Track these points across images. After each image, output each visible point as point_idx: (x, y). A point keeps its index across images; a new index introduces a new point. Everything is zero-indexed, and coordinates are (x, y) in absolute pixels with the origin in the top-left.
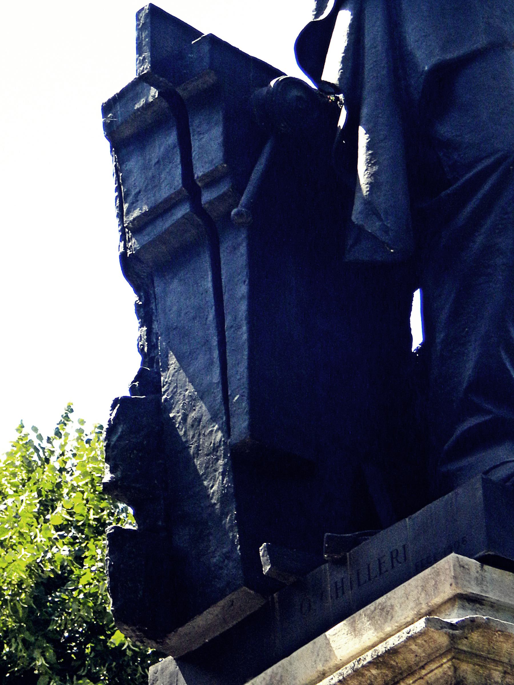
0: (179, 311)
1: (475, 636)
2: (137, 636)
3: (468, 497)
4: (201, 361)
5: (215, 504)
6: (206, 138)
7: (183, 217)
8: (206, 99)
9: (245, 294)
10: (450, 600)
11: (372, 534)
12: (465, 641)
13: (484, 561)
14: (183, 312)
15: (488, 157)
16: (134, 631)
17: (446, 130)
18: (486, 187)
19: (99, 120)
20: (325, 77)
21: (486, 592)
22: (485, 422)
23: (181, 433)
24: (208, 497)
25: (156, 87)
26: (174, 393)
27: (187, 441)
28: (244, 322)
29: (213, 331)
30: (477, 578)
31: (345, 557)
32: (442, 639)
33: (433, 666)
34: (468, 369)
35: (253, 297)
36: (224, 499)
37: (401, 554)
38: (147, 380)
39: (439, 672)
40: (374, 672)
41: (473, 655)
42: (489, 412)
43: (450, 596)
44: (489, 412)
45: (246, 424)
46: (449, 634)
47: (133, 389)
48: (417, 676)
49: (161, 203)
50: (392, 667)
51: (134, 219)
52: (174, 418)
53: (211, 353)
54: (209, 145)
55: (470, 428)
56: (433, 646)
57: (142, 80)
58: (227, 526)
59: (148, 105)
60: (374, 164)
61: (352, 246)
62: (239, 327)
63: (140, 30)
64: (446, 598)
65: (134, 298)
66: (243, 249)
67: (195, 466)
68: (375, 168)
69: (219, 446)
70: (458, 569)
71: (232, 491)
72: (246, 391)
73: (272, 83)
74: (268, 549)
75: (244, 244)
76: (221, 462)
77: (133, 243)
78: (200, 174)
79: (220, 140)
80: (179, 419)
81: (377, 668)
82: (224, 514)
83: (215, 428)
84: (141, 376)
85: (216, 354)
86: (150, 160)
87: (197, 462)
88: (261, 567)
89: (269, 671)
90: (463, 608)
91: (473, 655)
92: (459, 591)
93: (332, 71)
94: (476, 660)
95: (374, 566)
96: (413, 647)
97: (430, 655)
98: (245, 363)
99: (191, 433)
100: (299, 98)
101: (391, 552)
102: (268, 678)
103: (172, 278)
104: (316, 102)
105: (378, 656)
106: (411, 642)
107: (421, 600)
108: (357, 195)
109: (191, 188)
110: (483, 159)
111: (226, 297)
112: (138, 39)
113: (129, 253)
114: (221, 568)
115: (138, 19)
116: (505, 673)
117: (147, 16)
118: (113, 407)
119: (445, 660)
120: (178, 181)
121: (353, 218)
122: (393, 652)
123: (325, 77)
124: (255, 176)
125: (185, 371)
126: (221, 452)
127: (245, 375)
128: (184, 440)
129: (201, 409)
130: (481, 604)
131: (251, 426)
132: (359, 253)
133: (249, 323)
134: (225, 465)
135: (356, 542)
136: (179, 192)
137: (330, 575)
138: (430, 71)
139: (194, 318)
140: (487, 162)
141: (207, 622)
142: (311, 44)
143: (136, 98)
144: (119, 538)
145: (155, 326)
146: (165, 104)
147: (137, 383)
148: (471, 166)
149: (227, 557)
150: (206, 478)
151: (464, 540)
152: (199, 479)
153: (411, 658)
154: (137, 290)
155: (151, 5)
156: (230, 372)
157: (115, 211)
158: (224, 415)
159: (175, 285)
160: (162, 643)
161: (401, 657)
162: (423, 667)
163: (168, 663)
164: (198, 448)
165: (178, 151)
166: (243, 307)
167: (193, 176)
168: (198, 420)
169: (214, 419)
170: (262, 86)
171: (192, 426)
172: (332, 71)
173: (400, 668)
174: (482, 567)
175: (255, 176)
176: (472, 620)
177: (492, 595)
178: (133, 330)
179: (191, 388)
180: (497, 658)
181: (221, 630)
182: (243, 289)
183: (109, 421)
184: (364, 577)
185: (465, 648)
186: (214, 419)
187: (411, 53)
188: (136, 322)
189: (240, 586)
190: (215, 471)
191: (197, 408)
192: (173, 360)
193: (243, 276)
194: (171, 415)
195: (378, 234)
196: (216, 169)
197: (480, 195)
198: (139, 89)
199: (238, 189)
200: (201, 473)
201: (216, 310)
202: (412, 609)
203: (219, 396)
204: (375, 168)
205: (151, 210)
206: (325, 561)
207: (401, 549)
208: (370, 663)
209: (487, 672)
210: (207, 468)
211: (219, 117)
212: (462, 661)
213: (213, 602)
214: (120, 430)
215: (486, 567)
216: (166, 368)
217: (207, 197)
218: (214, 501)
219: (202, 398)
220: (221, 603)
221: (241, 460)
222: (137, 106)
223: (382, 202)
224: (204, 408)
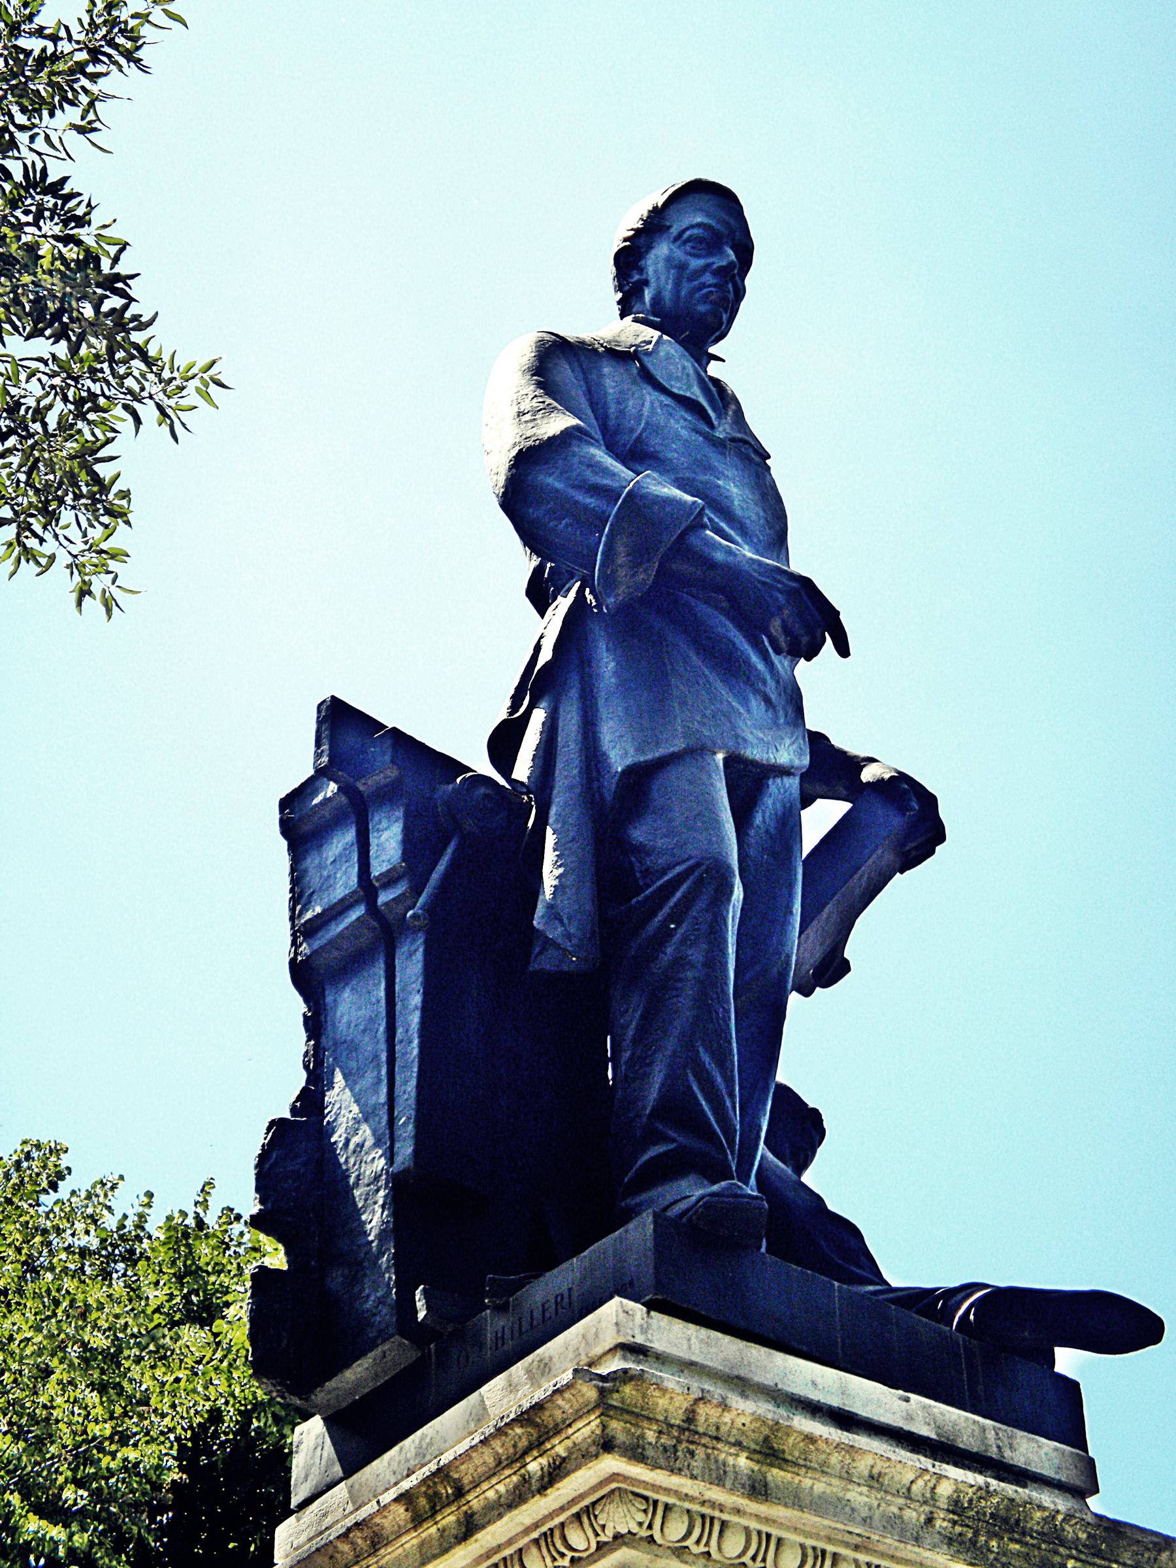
0: (349, 1023)
1: (628, 1390)
2: (278, 1391)
3: (639, 1233)
4: (369, 1078)
5: (372, 1241)
6: (385, 835)
7: (358, 919)
8: (387, 796)
9: (419, 1005)
10: (610, 1350)
11: (537, 1277)
12: (616, 1396)
13: (651, 1306)
14: (353, 1025)
15: (684, 861)
16: (274, 1385)
17: (639, 834)
18: (679, 894)
19: (276, 816)
20: (516, 775)
21: (651, 1341)
22: (666, 1153)
23: (342, 1160)
24: (366, 1234)
25: (335, 782)
26: (337, 1115)
27: (347, 1170)
28: (416, 1035)
29: (383, 1046)
30: (641, 1326)
31: (507, 1303)
32: (590, 1393)
33: (579, 1424)
34: (653, 1093)
35: (426, 1008)
36: (382, 1236)
37: (566, 1300)
38: (311, 1101)
39: (586, 1431)
40: (519, 1431)
41: (624, 1411)
42: (674, 1140)
43: (612, 1346)
44: (674, 1140)
45: (410, 1150)
46: (596, 1386)
47: (293, 1110)
48: (564, 1436)
49: (336, 904)
50: (537, 1426)
51: (306, 922)
52: (335, 1142)
53: (379, 1071)
54: (388, 842)
55: (652, 1158)
56: (581, 1400)
57: (321, 773)
58: (384, 1266)
59: (326, 800)
60: (560, 866)
61: (540, 953)
62: (410, 1042)
63: (320, 722)
64: (607, 1348)
65: (303, 1008)
66: (419, 955)
67: (354, 1198)
68: (561, 870)
69: (381, 1175)
70: (622, 1315)
71: (391, 1226)
72: (413, 1112)
73: (458, 780)
74: (424, 1291)
75: (421, 950)
76: (382, 1193)
77: (304, 948)
78: (377, 874)
79: (400, 838)
80: (340, 1145)
81: (522, 1427)
82: (381, 1253)
83: (378, 1156)
84: (304, 1095)
85: (384, 1071)
86: (326, 859)
87: (357, 1193)
88: (416, 1312)
89: (419, 1433)
90: (624, 1358)
91: (624, 1411)
92: (621, 1340)
93: (522, 770)
94: (627, 1417)
95: (537, 1314)
96: (560, 1402)
97: (577, 1411)
98: (413, 1083)
99: (352, 1161)
100: (486, 796)
101: (556, 1297)
102: (417, 1442)
103: (344, 987)
104: (507, 802)
105: (522, 1413)
106: (557, 1396)
107: (581, 1350)
108: (541, 897)
109: (367, 887)
110: (674, 867)
111: (398, 1007)
112: (317, 731)
113: (299, 958)
114: (374, 1315)
115: (319, 711)
116: (660, 1432)
117: (328, 707)
118: (269, 1129)
119: (593, 1417)
120: (354, 880)
121: (535, 922)
122: (538, 1407)
123: (516, 775)
124: (435, 876)
125: (351, 1090)
126: (382, 1182)
127: (413, 1094)
128: (344, 1167)
129: (366, 1131)
130: (646, 1355)
131: (416, 1152)
132: (545, 962)
133: (419, 1037)
134: (386, 1197)
135: (520, 1285)
136: (354, 892)
137: (492, 1324)
138: (623, 771)
139: (364, 1031)
140: (678, 869)
141: (357, 1375)
142: (504, 743)
143: (315, 793)
144: (263, 1276)
145: (323, 1040)
146: (343, 799)
147: (298, 1104)
148: (664, 873)
149: (380, 1301)
150: (364, 1212)
151: (631, 1283)
152: (358, 1212)
153: (558, 1415)
154: (306, 1001)
155: (333, 697)
156: (398, 1090)
157: (286, 914)
158: (388, 1140)
159: (346, 994)
160: (307, 1400)
161: (547, 1413)
162: (570, 1425)
163: (316, 1425)
164: (358, 1178)
165: (355, 848)
166: (415, 1019)
167: (369, 874)
168: (361, 1146)
169: (377, 1144)
170: (448, 783)
171: (354, 1152)
172: (522, 770)
173: (546, 1427)
174: (648, 1313)
175: (435, 876)
176: (625, 1371)
177: (658, 1345)
178: (298, 1042)
179: (355, 1109)
180: (651, 1416)
181: (371, 1385)
182: (417, 999)
183: (263, 1145)
184: (525, 1326)
185: (615, 1403)
186: (377, 1144)
187: (604, 754)
188: (303, 1035)
189: (392, 1336)
190: (375, 1203)
191: (360, 1132)
192: (338, 1077)
193: (418, 985)
194: (333, 1140)
195: (560, 941)
196: (393, 869)
197: (671, 903)
198: (317, 784)
199: (417, 891)
200: (360, 1205)
201: (387, 1023)
202: (571, 1361)
203: (385, 1118)
204: (561, 870)
205: (324, 912)
206: (486, 1307)
207: (566, 1294)
208: (513, 1420)
209: (639, 1432)
210: (366, 1200)
211: (400, 813)
212: (611, 1417)
213: (362, 1354)
214: (274, 1156)
215: (653, 1313)
216: (331, 1086)
217: (384, 898)
218: (371, 1238)
219: (366, 1120)
220: (371, 1355)
221: (403, 1190)
222: (315, 802)
223: (566, 905)
224: (369, 1132)
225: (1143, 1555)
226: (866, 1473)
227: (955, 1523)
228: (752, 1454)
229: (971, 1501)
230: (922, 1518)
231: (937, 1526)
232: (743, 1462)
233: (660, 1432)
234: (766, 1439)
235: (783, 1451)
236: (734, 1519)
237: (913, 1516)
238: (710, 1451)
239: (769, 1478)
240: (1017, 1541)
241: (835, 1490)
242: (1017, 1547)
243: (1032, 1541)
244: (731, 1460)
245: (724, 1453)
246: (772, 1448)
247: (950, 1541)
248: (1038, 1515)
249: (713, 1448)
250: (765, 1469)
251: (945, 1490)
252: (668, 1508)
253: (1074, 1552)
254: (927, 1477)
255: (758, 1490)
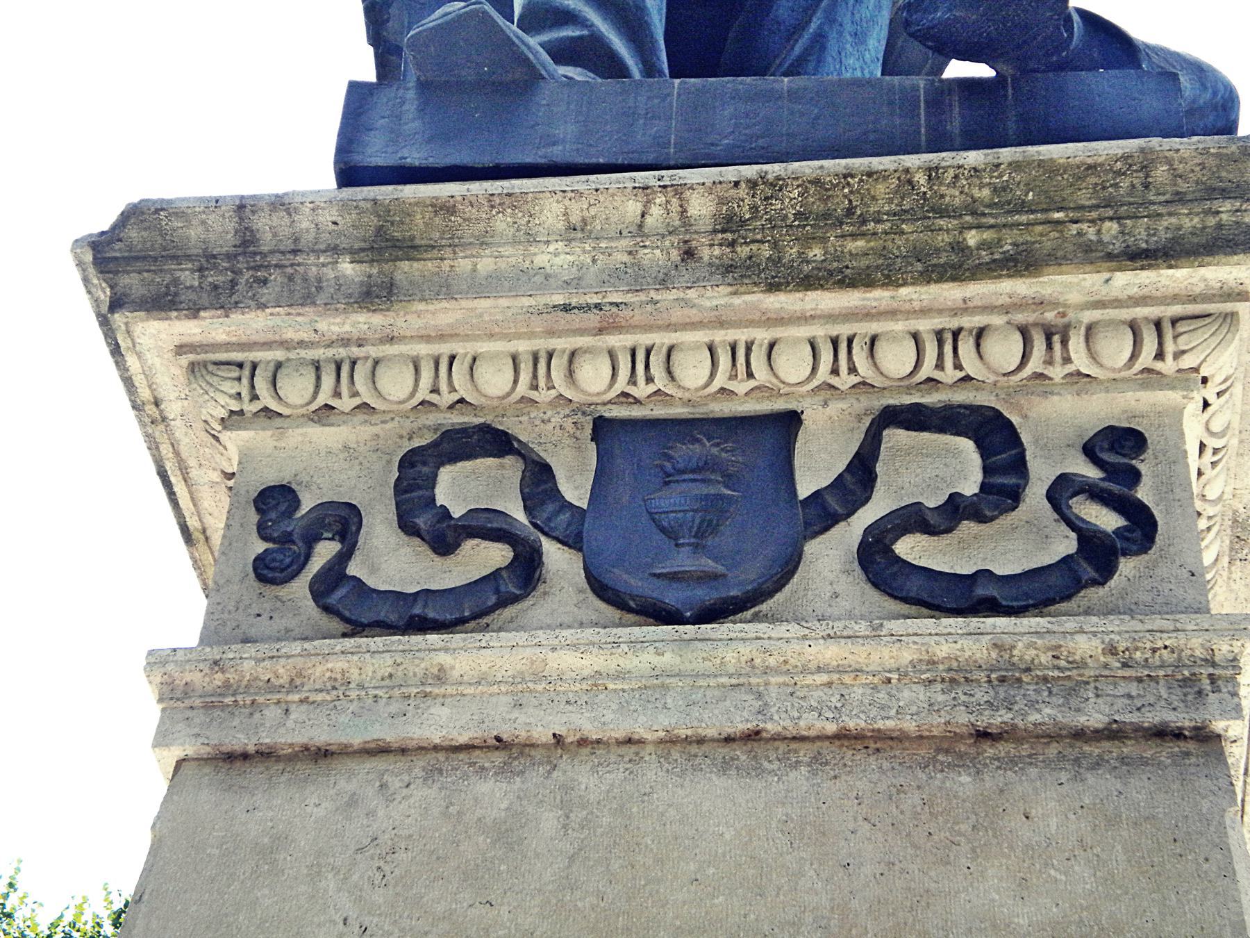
91: (135, 259)
209: (168, 279)
212: (116, 273)
225: (1116, 186)
226: (561, 225)
227: (732, 244)
228: (356, 255)
229: (754, 209)
230: (675, 255)
231: (706, 258)
232: (347, 267)
233: (201, 270)
234: (379, 230)
235: (412, 238)
236: (483, 347)
237: (655, 256)
238: (290, 270)
239: (398, 276)
240: (854, 236)
241: (513, 260)
242: (861, 243)
243: (880, 228)
244: (329, 273)
245: (312, 265)
246: (393, 239)
247: (729, 269)
248: (880, 189)
249: (292, 265)
250: (386, 267)
251: (701, 208)
252: (980, 334)
253: (968, 218)
254: (660, 199)
255: (375, 295)
